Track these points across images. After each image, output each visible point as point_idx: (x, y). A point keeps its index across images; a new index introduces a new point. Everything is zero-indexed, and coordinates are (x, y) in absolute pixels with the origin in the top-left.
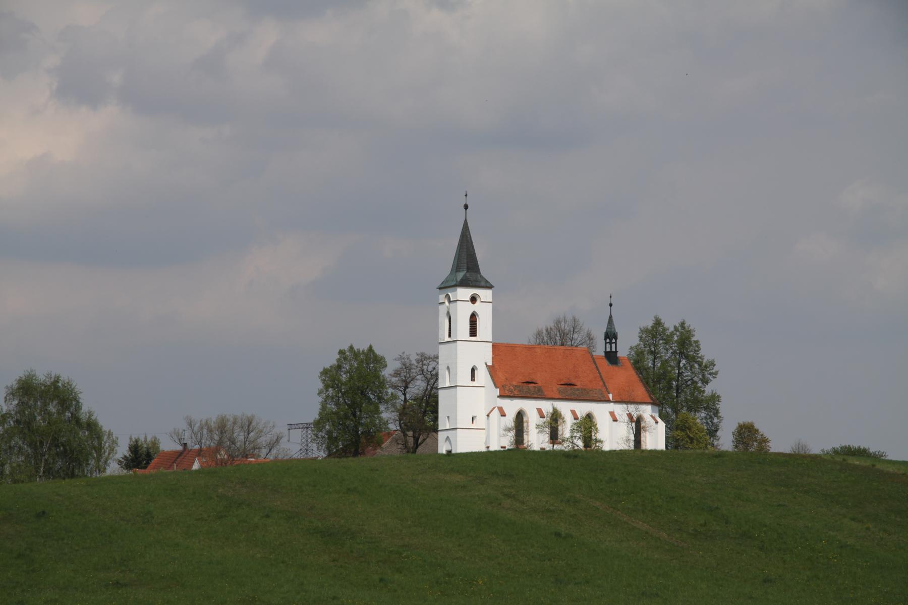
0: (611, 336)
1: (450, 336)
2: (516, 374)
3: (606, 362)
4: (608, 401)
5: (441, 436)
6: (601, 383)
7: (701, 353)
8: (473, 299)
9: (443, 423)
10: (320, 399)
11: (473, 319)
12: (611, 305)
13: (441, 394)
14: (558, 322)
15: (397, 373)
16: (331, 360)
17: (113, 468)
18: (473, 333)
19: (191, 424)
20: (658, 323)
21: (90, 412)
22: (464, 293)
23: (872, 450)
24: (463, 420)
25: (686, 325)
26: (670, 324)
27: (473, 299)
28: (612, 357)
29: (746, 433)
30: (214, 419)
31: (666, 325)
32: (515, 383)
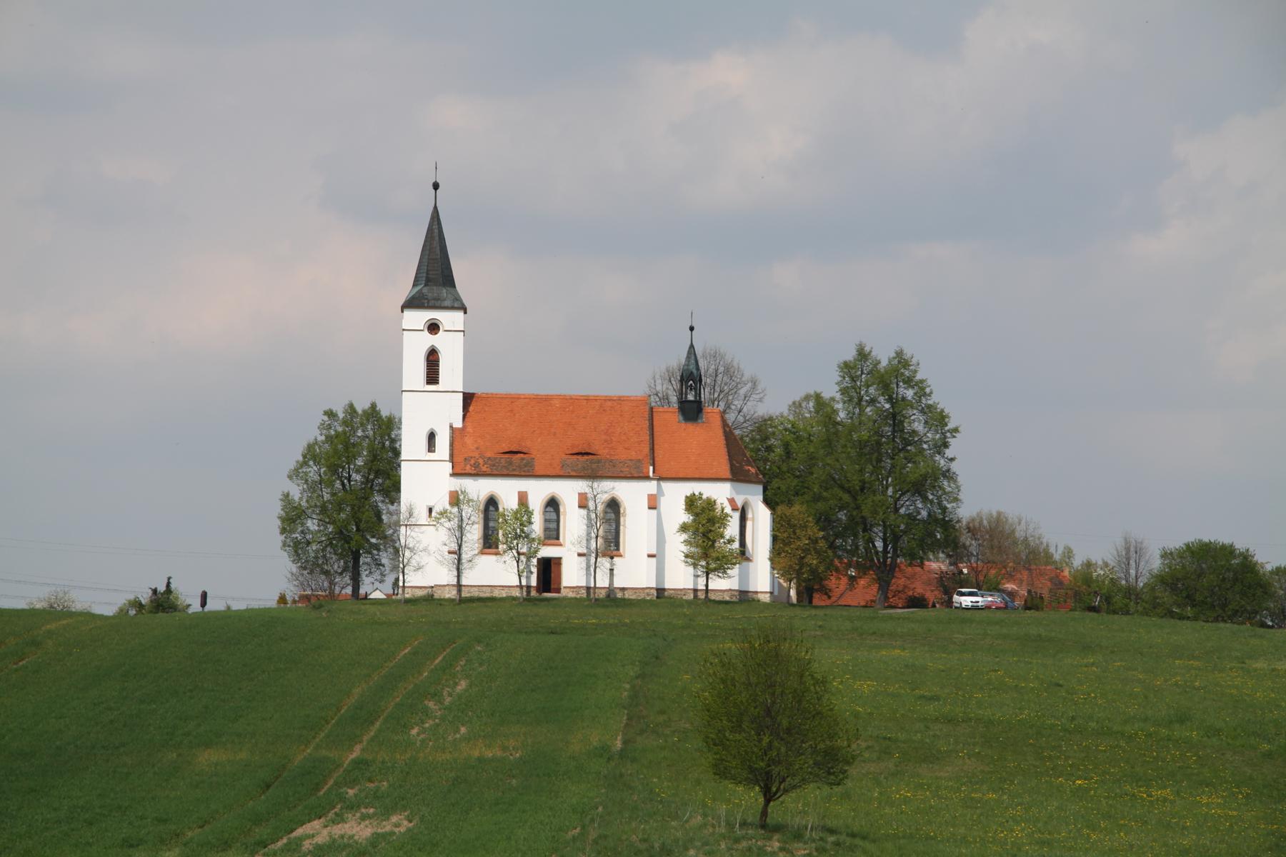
4: (647, 478)
6: (647, 450)
8: (433, 328)
11: (432, 359)
18: (432, 378)
22: (418, 318)
32: (489, 455)
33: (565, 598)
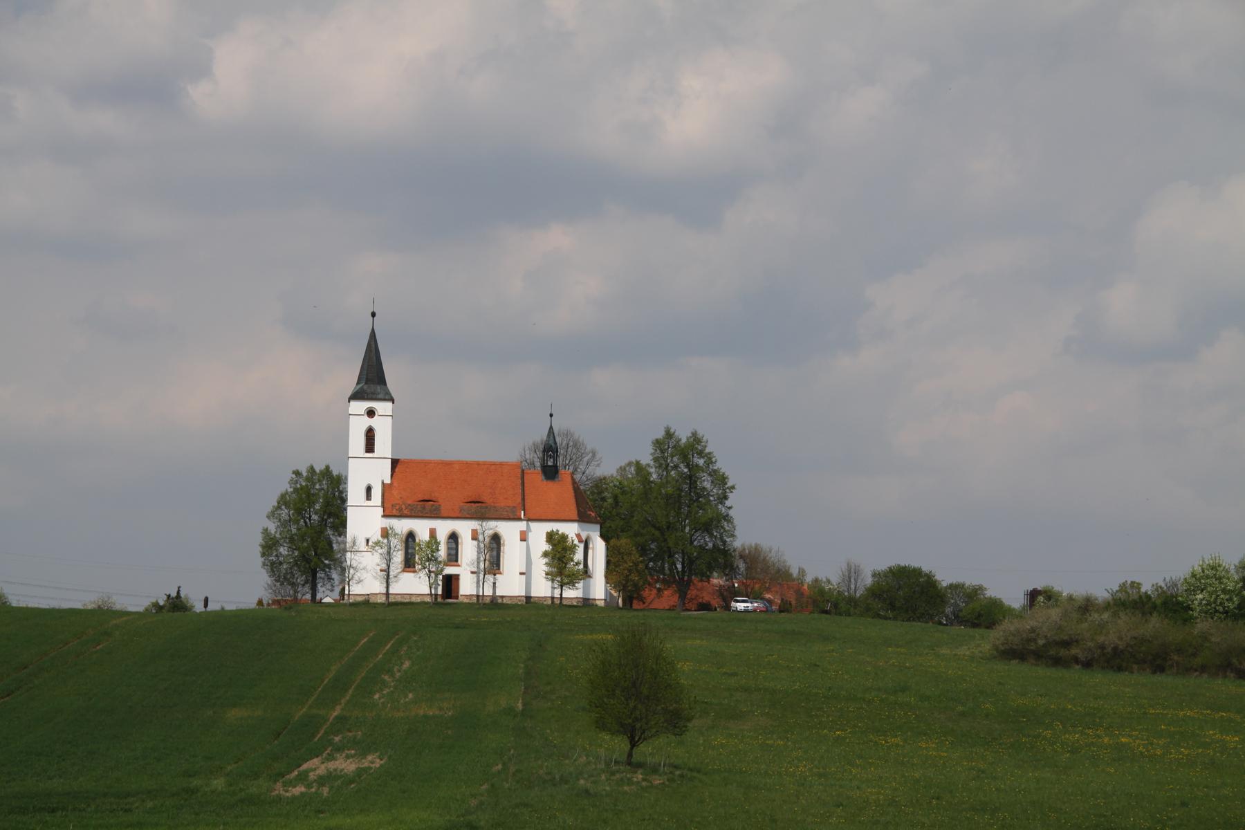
8: (371, 413)
11: (370, 435)
18: (370, 448)
22: (360, 407)
33: (462, 603)
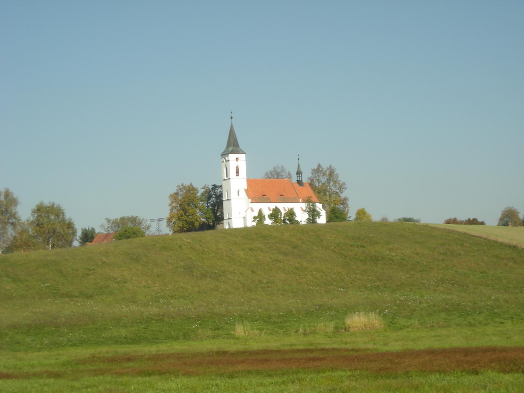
0: (299, 173)
1: (227, 176)
2: (257, 192)
3: (297, 185)
5: (225, 222)
7: (339, 179)
9: (226, 216)
10: (170, 208)
11: (237, 170)
12: (232, 118)
13: (224, 202)
14: (275, 168)
15: (203, 194)
16: (174, 190)
17: (76, 243)
18: (238, 175)
19: (109, 221)
20: (319, 166)
21: (70, 218)
23: (415, 219)
24: (234, 215)
25: (332, 166)
26: (325, 166)
27: (237, 159)
28: (300, 182)
29: (361, 213)
30: (119, 219)
31: (323, 167)
